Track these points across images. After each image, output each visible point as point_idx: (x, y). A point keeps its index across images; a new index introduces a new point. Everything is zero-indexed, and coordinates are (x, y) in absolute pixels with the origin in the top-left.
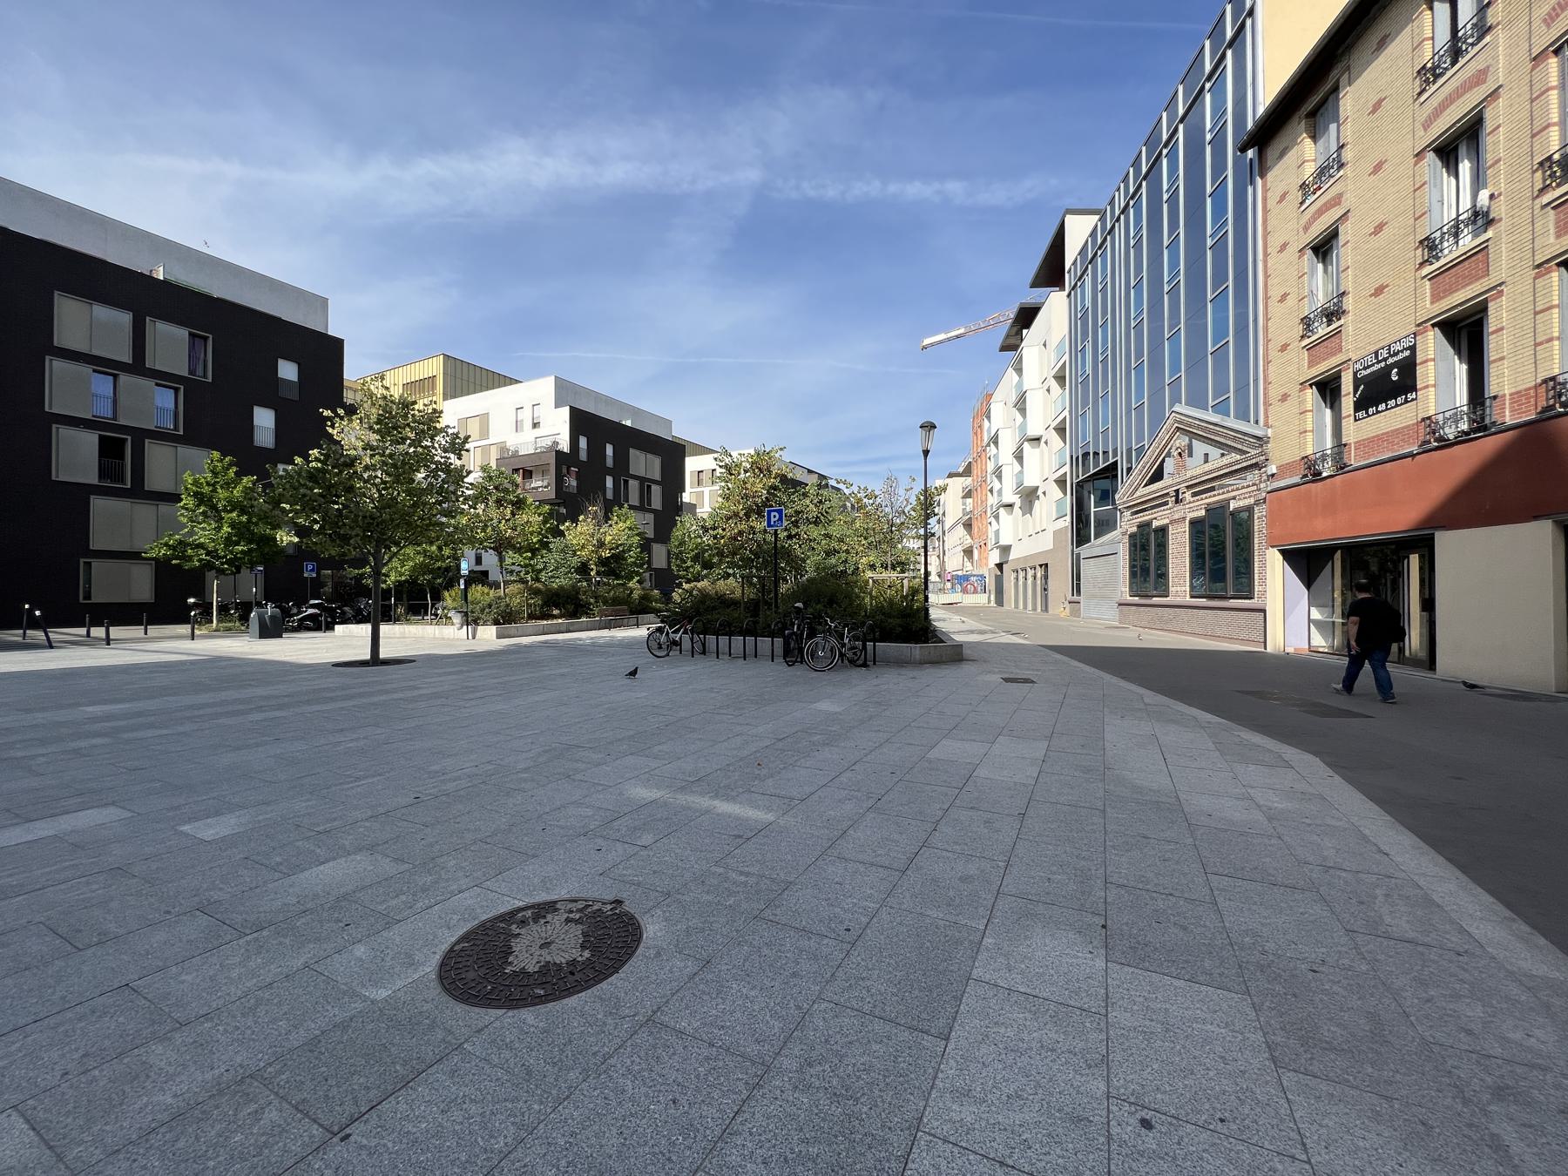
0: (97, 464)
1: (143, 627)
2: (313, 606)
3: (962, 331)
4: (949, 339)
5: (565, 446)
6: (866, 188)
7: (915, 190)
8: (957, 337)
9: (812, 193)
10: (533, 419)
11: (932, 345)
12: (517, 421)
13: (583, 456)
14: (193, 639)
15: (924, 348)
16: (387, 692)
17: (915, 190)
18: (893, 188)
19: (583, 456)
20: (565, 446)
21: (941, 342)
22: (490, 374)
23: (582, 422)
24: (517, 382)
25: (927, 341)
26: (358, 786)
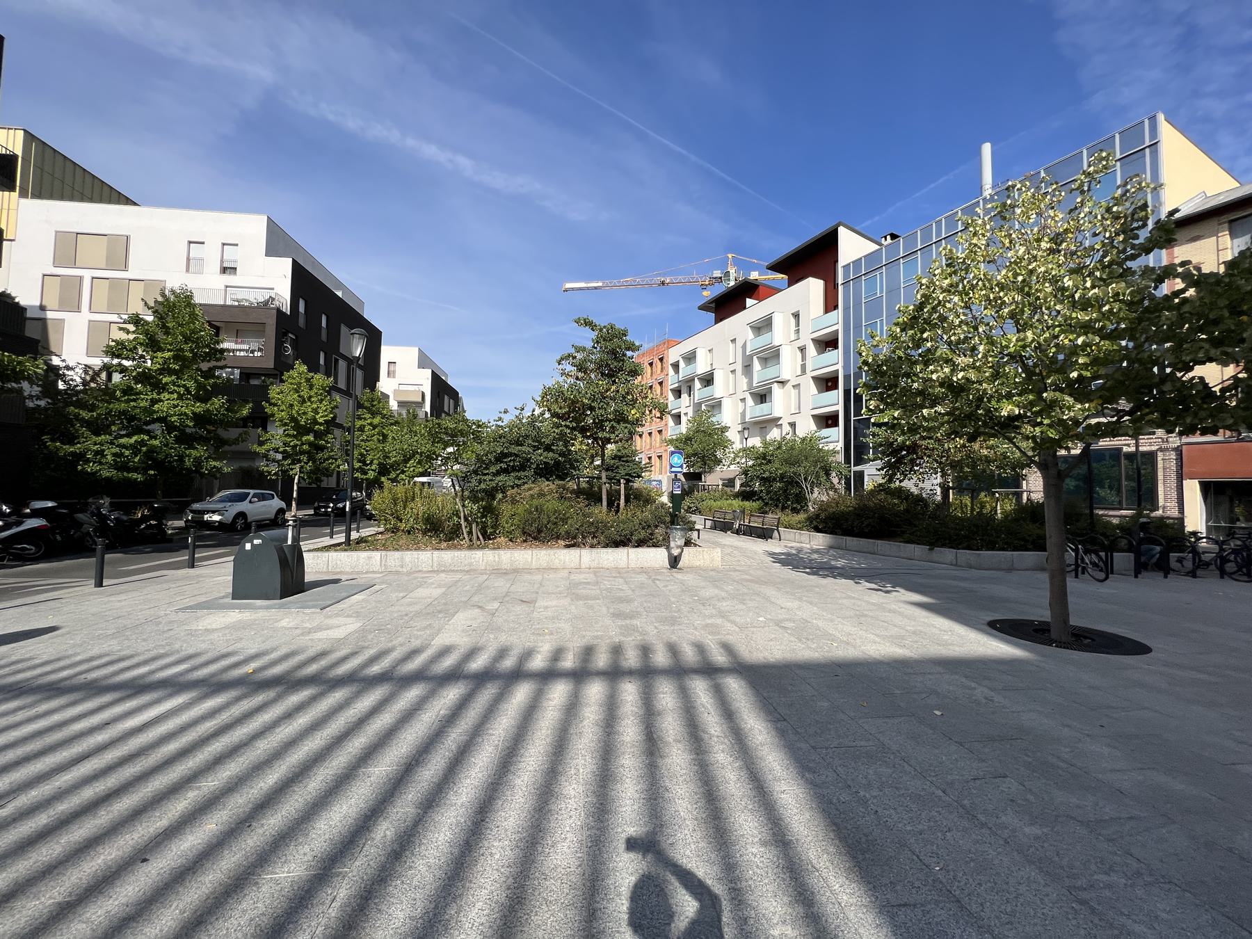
0: (54, 238)
1: (93, 560)
2: (36, 513)
3: (600, 284)
4: (588, 288)
5: (287, 309)
6: (382, 132)
7: (430, 151)
8: (596, 288)
9: (331, 117)
10: (222, 261)
11: (573, 289)
12: (188, 259)
13: (302, 322)
14: (193, 566)
15: (566, 291)
16: (29, 669)
17: (430, 151)
18: (411, 142)
19: (302, 322)
20: (287, 309)
21: (580, 289)
22: (87, 178)
23: (303, 280)
24: (128, 201)
25: (568, 285)
26: (901, 614)
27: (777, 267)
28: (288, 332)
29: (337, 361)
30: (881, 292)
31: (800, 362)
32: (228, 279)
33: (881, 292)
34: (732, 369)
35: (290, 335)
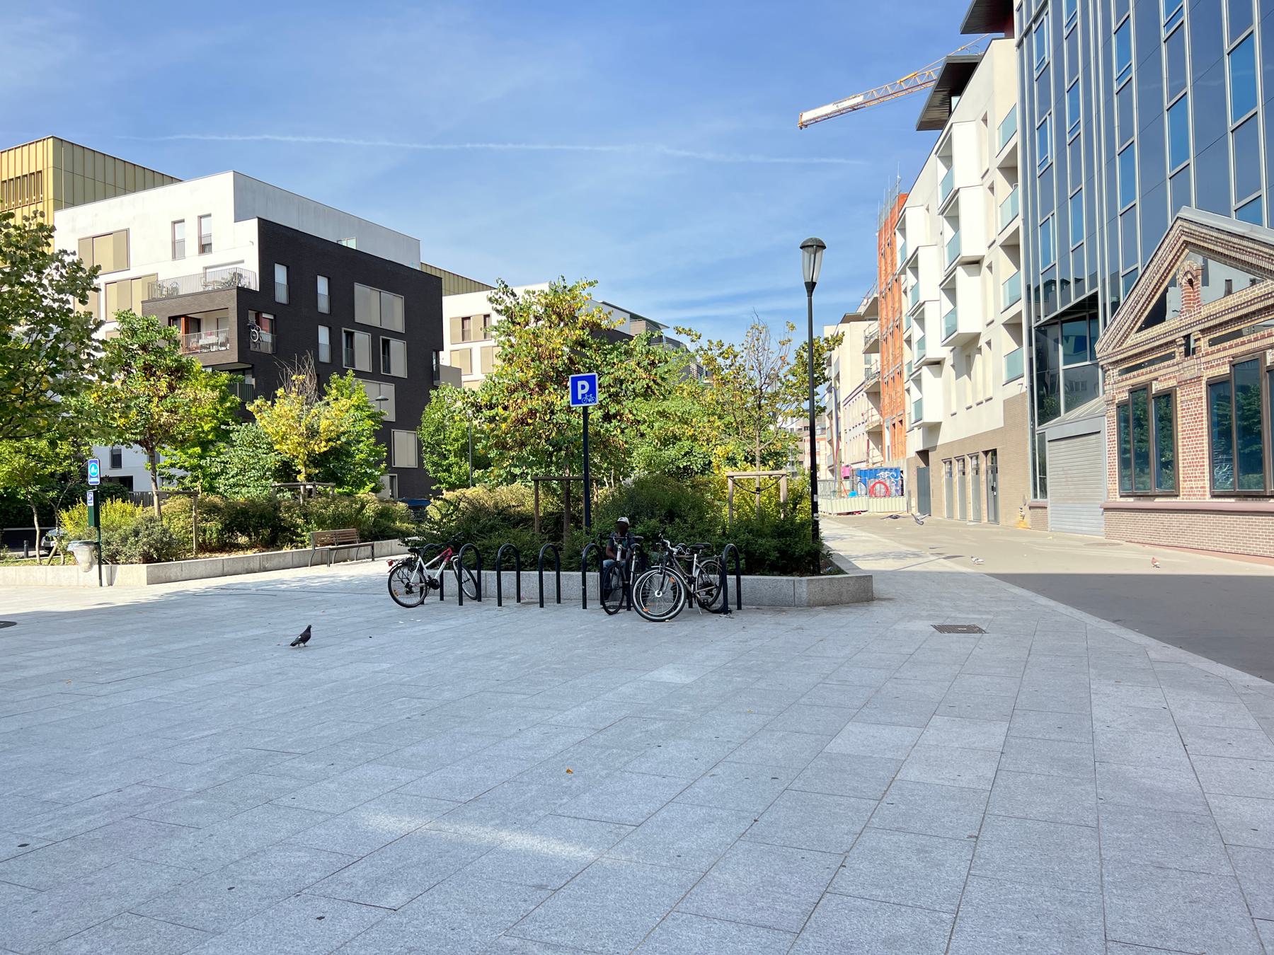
3: (860, 99)
4: (840, 112)
5: (253, 282)
8: (853, 108)
10: (200, 238)
11: (815, 121)
12: (174, 243)
13: (281, 295)
15: (804, 125)
19: (281, 295)
21: (828, 117)
25: (807, 116)
27: (969, 28)
28: (261, 312)
29: (350, 336)
30: (1054, 259)
31: (860, 555)
32: (208, 259)
33: (1054, 259)
34: (1222, 288)
35: (264, 315)
